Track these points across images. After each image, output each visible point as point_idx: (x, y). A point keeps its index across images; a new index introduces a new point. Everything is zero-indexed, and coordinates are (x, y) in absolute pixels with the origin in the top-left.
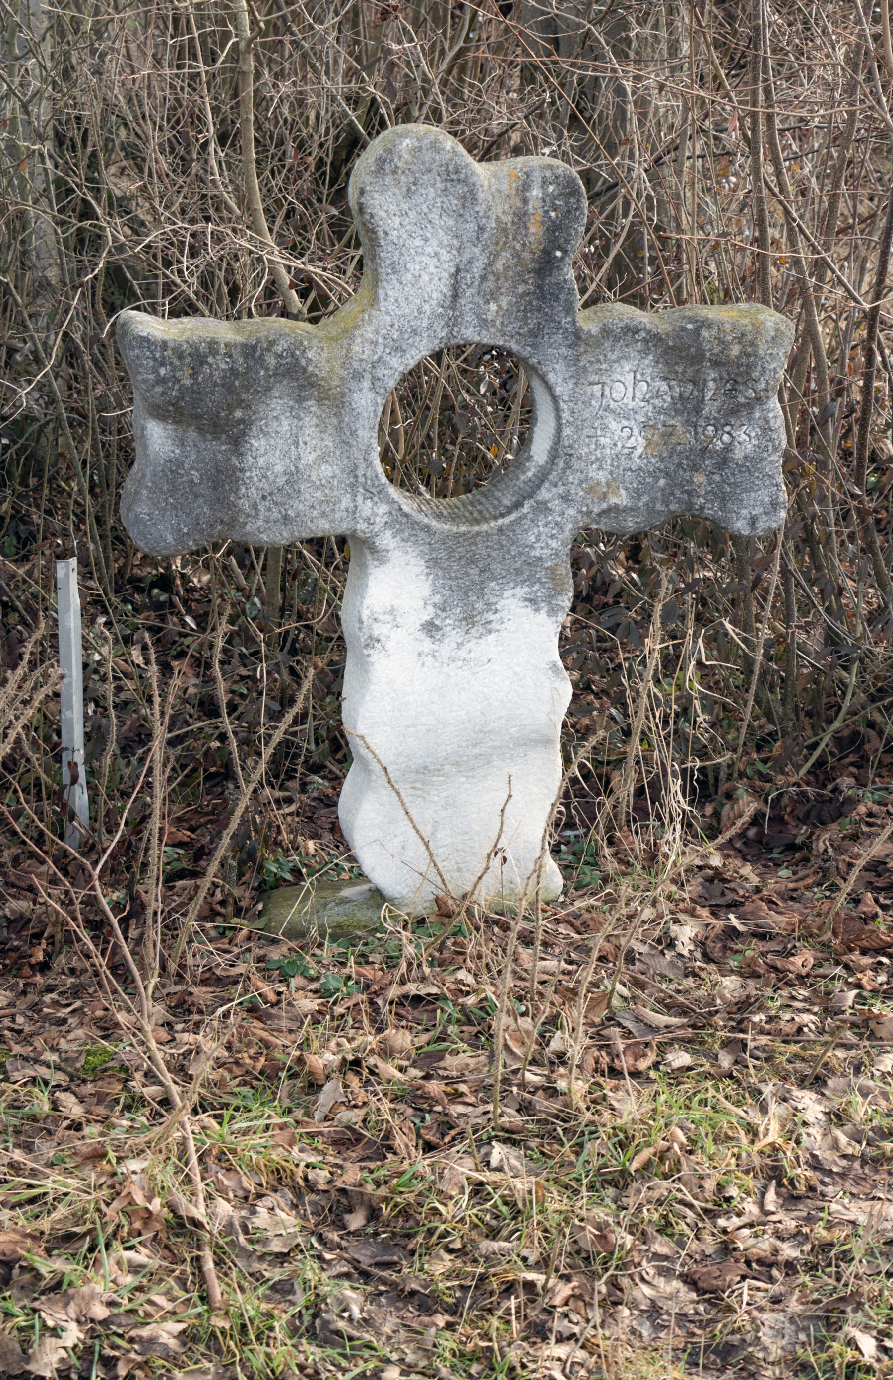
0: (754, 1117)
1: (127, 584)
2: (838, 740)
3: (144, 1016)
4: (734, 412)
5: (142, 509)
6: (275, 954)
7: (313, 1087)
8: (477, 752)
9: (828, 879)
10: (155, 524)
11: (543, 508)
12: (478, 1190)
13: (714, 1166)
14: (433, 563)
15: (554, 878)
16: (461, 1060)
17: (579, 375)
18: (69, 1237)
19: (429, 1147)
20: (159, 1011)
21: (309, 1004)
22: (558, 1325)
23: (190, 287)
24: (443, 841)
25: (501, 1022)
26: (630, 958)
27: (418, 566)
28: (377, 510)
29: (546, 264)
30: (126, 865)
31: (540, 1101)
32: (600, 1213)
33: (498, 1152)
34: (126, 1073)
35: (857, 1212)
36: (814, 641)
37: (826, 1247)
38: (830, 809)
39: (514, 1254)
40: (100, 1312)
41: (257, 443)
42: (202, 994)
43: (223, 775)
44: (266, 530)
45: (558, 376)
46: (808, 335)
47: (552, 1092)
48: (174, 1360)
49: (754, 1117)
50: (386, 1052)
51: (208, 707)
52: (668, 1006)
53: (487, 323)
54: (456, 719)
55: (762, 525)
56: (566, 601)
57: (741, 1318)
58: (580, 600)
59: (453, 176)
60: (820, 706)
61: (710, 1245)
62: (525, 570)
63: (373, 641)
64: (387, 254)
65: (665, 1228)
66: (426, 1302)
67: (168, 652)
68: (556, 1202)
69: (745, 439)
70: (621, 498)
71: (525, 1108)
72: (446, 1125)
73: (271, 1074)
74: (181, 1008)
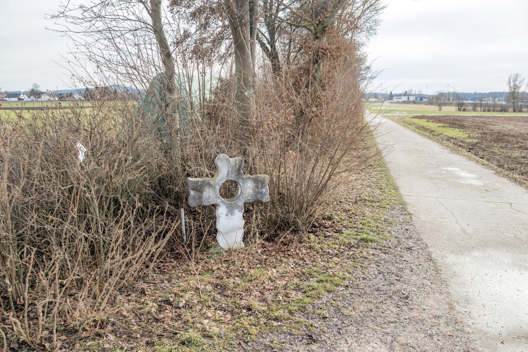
0: (268, 272)
1: (191, 212)
2: (278, 227)
3: (192, 264)
4: (263, 187)
5: (190, 201)
6: (209, 256)
7: (214, 271)
8: (233, 230)
9: (276, 243)
10: (192, 203)
11: (240, 199)
12: (234, 283)
13: (263, 278)
14: (227, 207)
15: (243, 245)
16: (232, 267)
17: (244, 183)
18: (183, 290)
19: (228, 278)
20: (195, 263)
21: (213, 262)
22: (244, 298)
23: (196, 174)
24: (229, 241)
25: (236, 262)
26: (252, 254)
27: (225, 207)
28: (219, 200)
29: (239, 170)
30: (190, 246)
31: (241, 272)
32: (249, 285)
33: (236, 278)
34: (190, 271)
35: (280, 283)
36: (274, 215)
37: (276, 287)
38: (277, 235)
39: (238, 290)
40: (187, 299)
41: (204, 193)
42: (200, 261)
43: (202, 235)
44: (206, 204)
45: (241, 183)
46: (272, 179)
47: (243, 270)
48: (197, 304)
49: (268, 272)
50: (223, 267)
51: (200, 226)
52: (257, 260)
53: (232, 177)
54: (230, 225)
55: (267, 201)
56: (243, 211)
57: (266, 296)
58: (245, 212)
59: (227, 160)
60: (275, 223)
61: (262, 288)
62: (238, 207)
63: (220, 217)
64: (219, 169)
65: (257, 286)
66: (227, 296)
67: (194, 219)
68: (243, 284)
69: (264, 190)
70: (249, 198)
71: (240, 273)
72: (230, 275)
73: (208, 270)
74: (197, 263)
